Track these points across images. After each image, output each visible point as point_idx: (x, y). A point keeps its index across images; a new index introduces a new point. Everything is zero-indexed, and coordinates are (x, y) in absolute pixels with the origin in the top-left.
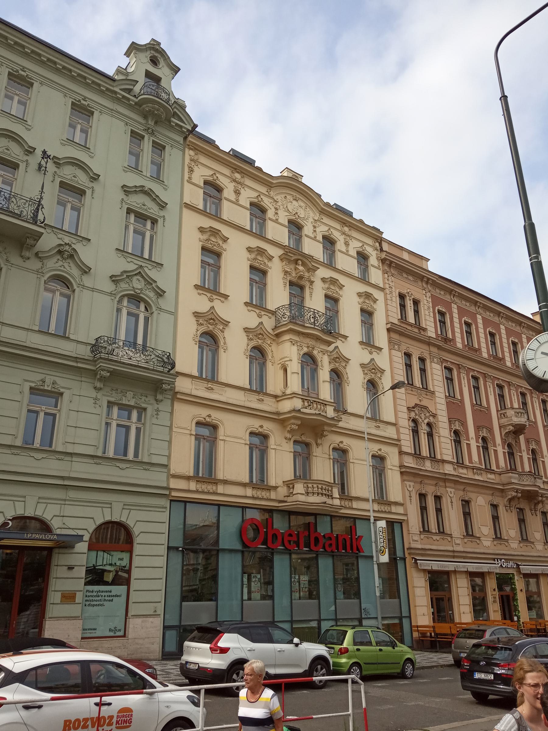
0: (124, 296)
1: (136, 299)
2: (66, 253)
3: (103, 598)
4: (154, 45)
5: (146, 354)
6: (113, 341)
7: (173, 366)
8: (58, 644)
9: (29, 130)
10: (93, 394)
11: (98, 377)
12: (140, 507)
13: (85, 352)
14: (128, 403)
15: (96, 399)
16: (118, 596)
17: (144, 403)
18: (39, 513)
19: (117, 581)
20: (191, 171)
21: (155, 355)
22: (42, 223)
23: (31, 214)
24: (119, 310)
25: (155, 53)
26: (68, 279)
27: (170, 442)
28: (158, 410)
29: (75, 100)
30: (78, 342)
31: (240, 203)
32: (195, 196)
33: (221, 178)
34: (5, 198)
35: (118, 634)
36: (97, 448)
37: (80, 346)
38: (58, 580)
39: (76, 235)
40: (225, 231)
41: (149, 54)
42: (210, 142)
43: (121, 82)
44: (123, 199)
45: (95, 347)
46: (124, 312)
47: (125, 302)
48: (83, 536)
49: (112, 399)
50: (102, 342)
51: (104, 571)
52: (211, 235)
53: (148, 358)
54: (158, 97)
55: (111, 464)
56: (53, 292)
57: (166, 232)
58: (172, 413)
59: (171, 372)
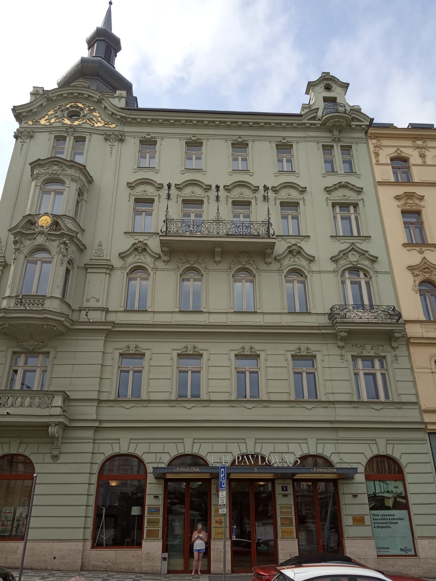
0: (344, 270)
1: (355, 270)
2: (295, 251)
3: (388, 521)
4: (324, 76)
5: (373, 311)
6: (345, 306)
7: (400, 315)
8: (348, 561)
9: (252, 175)
10: (338, 352)
11: (339, 338)
12: (274, 441)
13: (324, 320)
14: (368, 354)
15: (342, 355)
16: (401, 519)
17: (381, 352)
18: (320, 451)
19: (397, 506)
20: (377, 155)
21: (381, 310)
22: (273, 235)
23: (265, 232)
24: (343, 282)
25: (328, 81)
26: (299, 269)
27: (414, 382)
28: (396, 356)
29: (278, 142)
30: (318, 314)
31: (428, 163)
32: (386, 173)
33: (403, 150)
34: (246, 227)
35: (409, 553)
36: (353, 395)
37: (319, 317)
38: (347, 506)
39: (299, 236)
40: (419, 191)
41: (322, 85)
42: (390, 126)
43: (307, 115)
44: (327, 198)
45: (331, 315)
46: (348, 282)
47: (347, 275)
48: (357, 468)
49: (355, 354)
50: (335, 310)
51: (384, 497)
52: (407, 199)
53: (376, 314)
54: (336, 112)
55: (367, 407)
56: (292, 282)
57: (367, 211)
58: (409, 356)
59: (400, 321)
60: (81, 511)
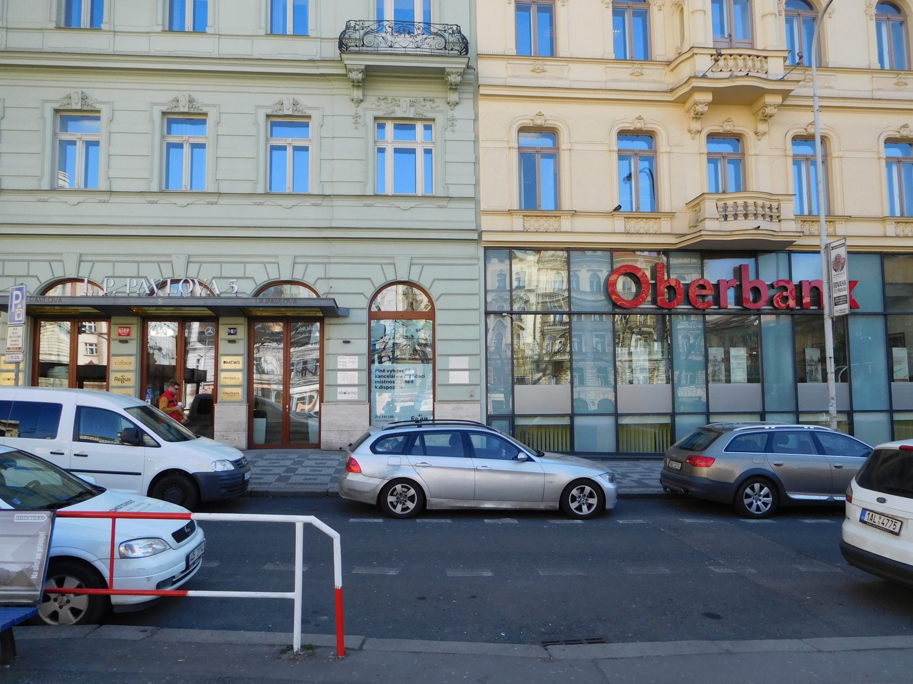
49: (380, 114)
60: (240, 359)
